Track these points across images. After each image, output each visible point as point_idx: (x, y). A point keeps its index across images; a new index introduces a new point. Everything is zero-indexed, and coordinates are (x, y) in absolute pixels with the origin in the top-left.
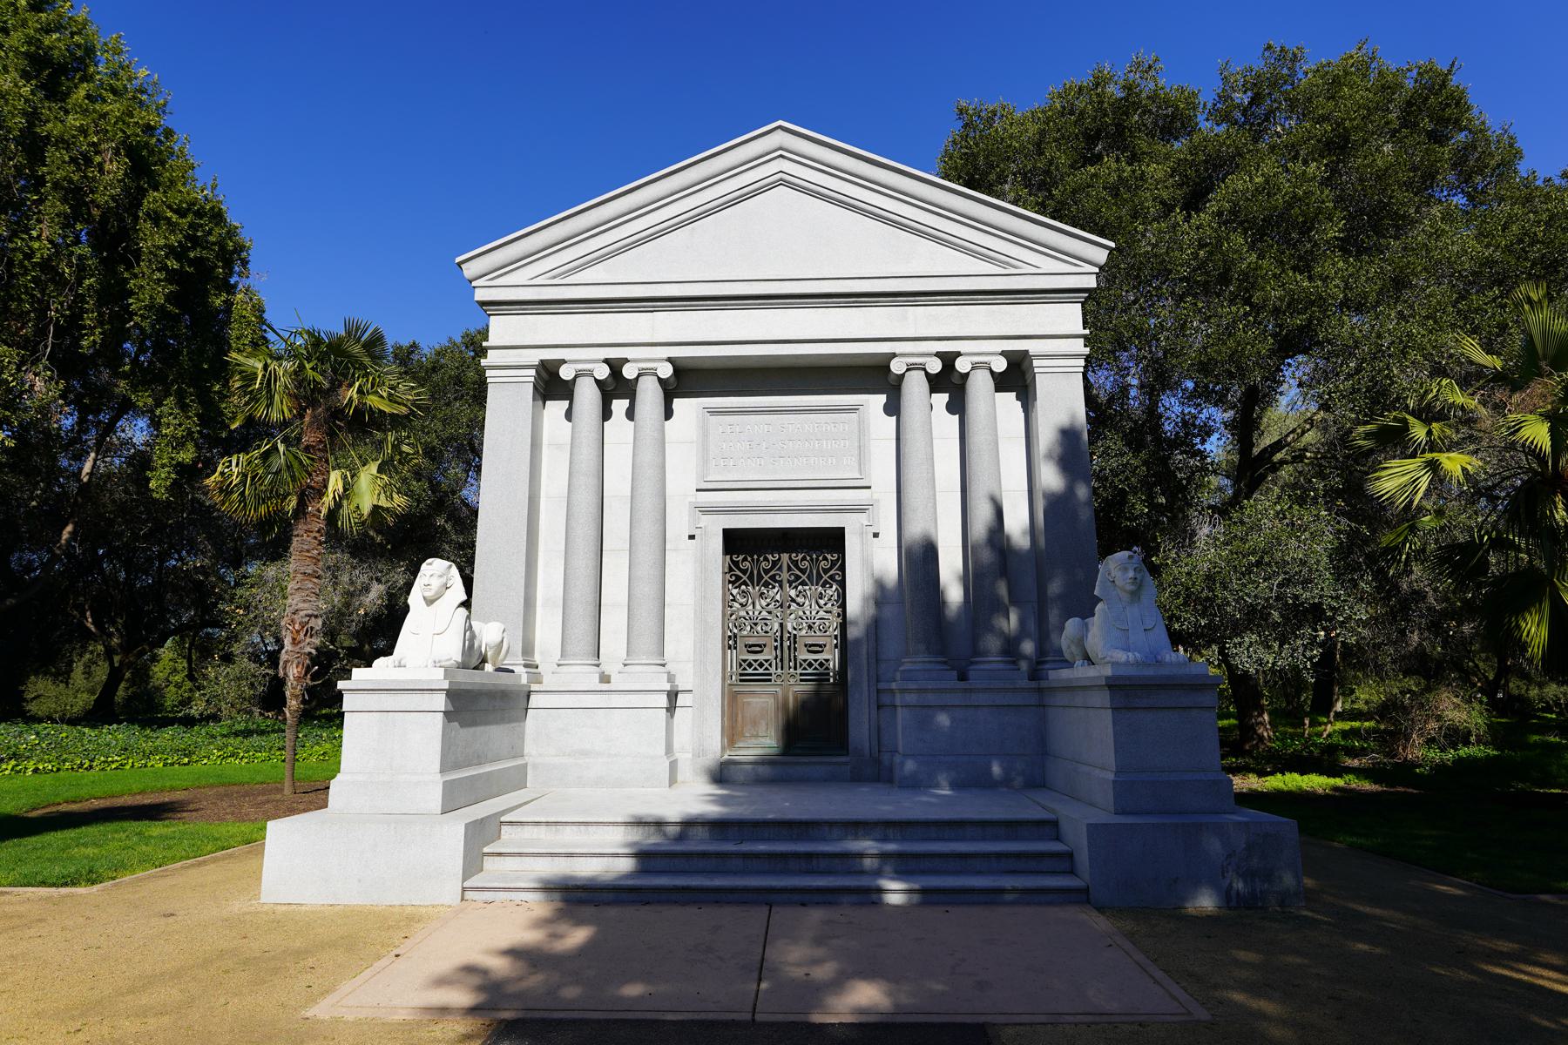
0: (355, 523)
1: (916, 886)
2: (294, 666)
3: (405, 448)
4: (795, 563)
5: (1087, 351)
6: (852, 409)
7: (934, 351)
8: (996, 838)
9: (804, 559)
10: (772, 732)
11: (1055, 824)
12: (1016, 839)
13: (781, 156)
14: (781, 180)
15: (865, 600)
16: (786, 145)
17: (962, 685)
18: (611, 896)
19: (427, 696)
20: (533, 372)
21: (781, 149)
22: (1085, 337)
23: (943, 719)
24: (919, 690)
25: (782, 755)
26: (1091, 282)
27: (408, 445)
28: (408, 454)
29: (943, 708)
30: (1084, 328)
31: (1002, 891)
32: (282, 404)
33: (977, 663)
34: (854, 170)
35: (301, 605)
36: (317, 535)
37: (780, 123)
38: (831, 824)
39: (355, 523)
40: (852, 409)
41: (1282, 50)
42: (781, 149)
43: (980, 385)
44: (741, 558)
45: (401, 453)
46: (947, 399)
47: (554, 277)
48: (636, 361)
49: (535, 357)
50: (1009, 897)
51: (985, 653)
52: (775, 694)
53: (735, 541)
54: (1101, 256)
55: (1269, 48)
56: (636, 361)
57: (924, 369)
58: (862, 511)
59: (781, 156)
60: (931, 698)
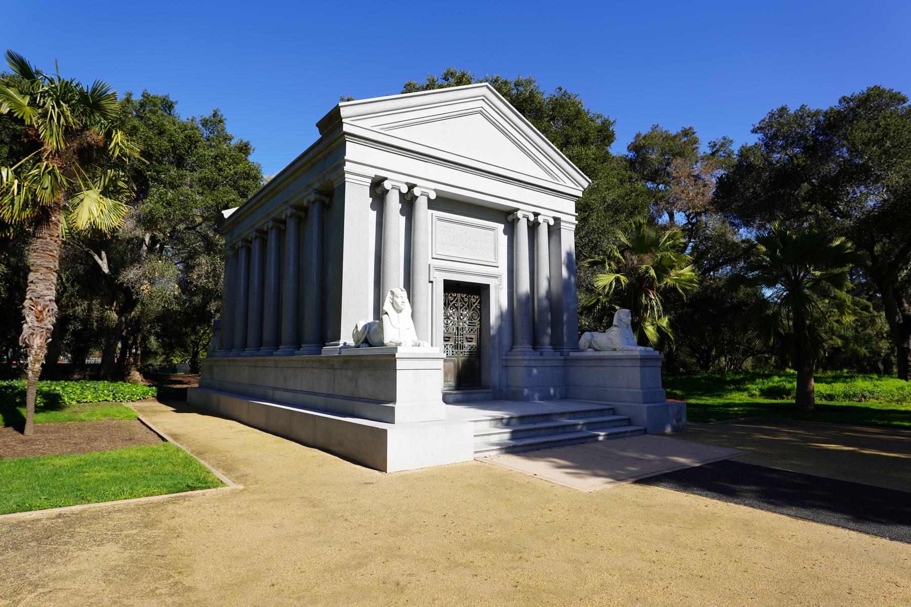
0: (66, 233)
1: (607, 433)
2: (38, 338)
3: (121, 184)
4: (463, 298)
5: (577, 222)
6: (492, 229)
7: (434, 188)
8: (598, 416)
9: (466, 297)
10: (453, 379)
11: (613, 409)
12: (604, 416)
13: (483, 100)
14: (481, 111)
15: (496, 318)
16: (486, 95)
17: (542, 358)
18: (521, 449)
19: (435, 361)
20: (370, 181)
21: (484, 96)
22: (576, 216)
23: (535, 371)
24: (529, 360)
25: (456, 390)
26: (580, 194)
27: (124, 181)
28: (122, 188)
29: (536, 367)
30: (576, 212)
31: (627, 432)
32: (58, 136)
33: (541, 348)
34: (448, 99)
35: (45, 292)
36: (57, 239)
37: (487, 84)
38: (555, 414)
39: (66, 233)
40: (492, 229)
41: (565, 92)
42: (484, 96)
43: (422, 204)
44: (465, 295)
45: (116, 186)
46: (503, 227)
47: (382, 129)
48: (420, 187)
49: (373, 173)
50: (628, 434)
51: (543, 345)
52: (454, 361)
53: (450, 287)
54: (586, 185)
55: (560, 89)
56: (420, 187)
57: (399, 190)
58: (496, 277)
59: (483, 100)
60: (533, 363)
